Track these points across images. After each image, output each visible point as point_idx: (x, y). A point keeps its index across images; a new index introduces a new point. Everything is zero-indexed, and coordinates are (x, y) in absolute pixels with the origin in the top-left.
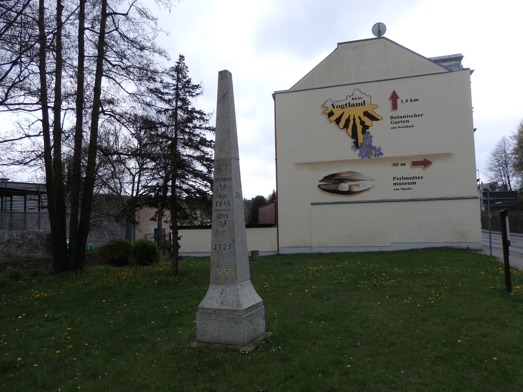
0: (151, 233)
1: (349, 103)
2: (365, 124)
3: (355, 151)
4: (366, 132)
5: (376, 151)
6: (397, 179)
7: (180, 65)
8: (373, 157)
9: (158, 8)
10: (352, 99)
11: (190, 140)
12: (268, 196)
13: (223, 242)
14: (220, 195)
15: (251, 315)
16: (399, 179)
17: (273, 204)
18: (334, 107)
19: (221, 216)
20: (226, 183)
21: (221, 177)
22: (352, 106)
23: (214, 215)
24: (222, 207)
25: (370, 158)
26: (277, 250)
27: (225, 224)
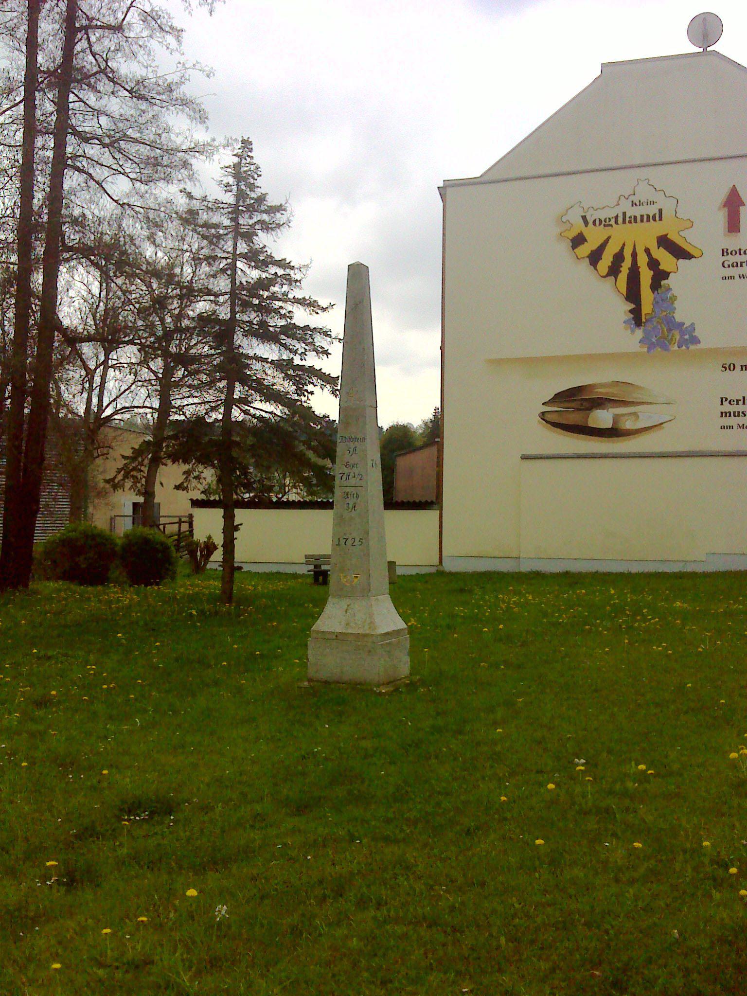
0: (125, 514)
1: (624, 214)
2: (661, 267)
3: (633, 332)
4: (660, 286)
5: (683, 334)
6: (730, 402)
7: (244, 161)
8: (676, 347)
9: (185, 11)
10: (631, 205)
11: (263, 324)
12: (420, 423)
15: (389, 644)
16: (735, 402)
17: (434, 450)
18: (586, 223)
19: (348, 494)
22: (630, 222)
23: (338, 492)
25: (667, 350)
26: (436, 561)
27: (355, 507)
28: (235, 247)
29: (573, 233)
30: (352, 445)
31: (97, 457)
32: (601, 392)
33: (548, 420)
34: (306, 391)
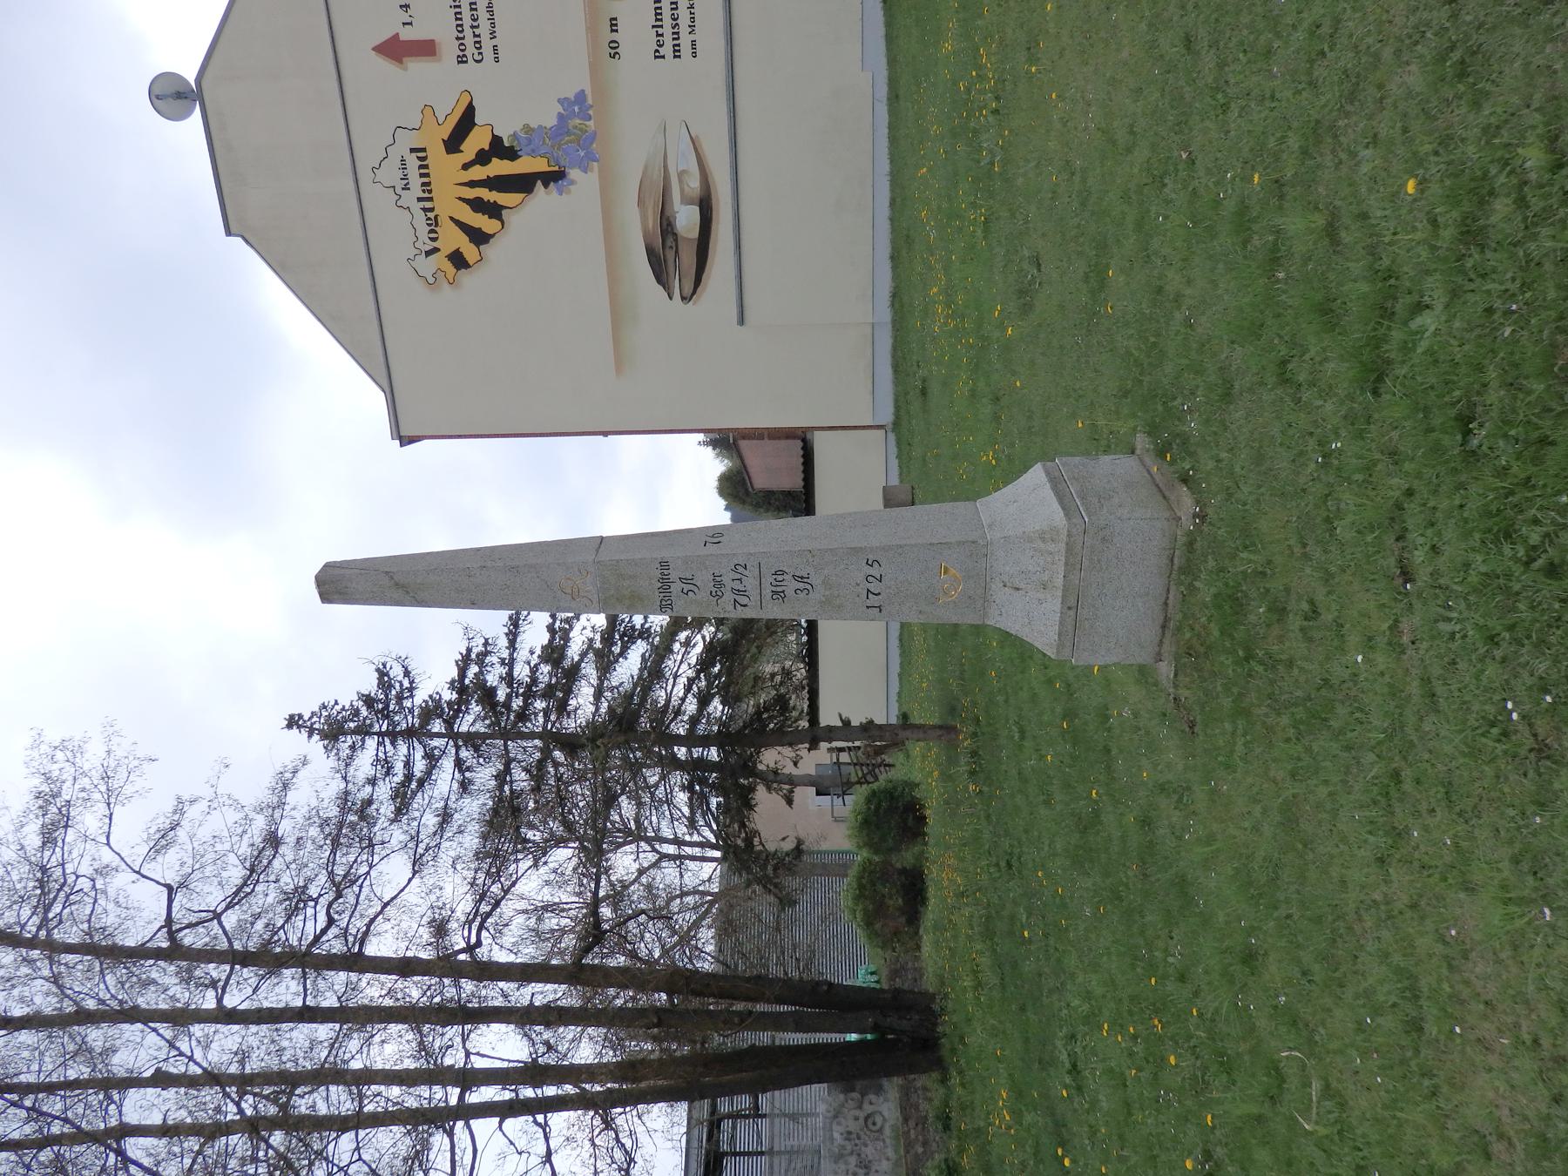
1: (420, 200)
2: (487, 148)
3: (572, 182)
5: (573, 115)
7: (316, 726)
8: (591, 123)
11: (548, 693)
13: (858, 585)
14: (714, 594)
18: (436, 250)
20: (674, 576)
21: (657, 593)
24: (748, 588)
27: (802, 578)
28: (439, 735)
29: (449, 267)
30: (676, 588)
31: (763, 846)
32: (653, 222)
33: (691, 291)
34: (642, 625)
